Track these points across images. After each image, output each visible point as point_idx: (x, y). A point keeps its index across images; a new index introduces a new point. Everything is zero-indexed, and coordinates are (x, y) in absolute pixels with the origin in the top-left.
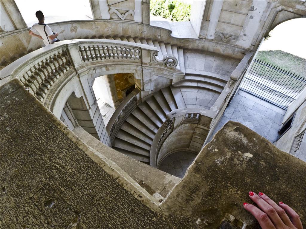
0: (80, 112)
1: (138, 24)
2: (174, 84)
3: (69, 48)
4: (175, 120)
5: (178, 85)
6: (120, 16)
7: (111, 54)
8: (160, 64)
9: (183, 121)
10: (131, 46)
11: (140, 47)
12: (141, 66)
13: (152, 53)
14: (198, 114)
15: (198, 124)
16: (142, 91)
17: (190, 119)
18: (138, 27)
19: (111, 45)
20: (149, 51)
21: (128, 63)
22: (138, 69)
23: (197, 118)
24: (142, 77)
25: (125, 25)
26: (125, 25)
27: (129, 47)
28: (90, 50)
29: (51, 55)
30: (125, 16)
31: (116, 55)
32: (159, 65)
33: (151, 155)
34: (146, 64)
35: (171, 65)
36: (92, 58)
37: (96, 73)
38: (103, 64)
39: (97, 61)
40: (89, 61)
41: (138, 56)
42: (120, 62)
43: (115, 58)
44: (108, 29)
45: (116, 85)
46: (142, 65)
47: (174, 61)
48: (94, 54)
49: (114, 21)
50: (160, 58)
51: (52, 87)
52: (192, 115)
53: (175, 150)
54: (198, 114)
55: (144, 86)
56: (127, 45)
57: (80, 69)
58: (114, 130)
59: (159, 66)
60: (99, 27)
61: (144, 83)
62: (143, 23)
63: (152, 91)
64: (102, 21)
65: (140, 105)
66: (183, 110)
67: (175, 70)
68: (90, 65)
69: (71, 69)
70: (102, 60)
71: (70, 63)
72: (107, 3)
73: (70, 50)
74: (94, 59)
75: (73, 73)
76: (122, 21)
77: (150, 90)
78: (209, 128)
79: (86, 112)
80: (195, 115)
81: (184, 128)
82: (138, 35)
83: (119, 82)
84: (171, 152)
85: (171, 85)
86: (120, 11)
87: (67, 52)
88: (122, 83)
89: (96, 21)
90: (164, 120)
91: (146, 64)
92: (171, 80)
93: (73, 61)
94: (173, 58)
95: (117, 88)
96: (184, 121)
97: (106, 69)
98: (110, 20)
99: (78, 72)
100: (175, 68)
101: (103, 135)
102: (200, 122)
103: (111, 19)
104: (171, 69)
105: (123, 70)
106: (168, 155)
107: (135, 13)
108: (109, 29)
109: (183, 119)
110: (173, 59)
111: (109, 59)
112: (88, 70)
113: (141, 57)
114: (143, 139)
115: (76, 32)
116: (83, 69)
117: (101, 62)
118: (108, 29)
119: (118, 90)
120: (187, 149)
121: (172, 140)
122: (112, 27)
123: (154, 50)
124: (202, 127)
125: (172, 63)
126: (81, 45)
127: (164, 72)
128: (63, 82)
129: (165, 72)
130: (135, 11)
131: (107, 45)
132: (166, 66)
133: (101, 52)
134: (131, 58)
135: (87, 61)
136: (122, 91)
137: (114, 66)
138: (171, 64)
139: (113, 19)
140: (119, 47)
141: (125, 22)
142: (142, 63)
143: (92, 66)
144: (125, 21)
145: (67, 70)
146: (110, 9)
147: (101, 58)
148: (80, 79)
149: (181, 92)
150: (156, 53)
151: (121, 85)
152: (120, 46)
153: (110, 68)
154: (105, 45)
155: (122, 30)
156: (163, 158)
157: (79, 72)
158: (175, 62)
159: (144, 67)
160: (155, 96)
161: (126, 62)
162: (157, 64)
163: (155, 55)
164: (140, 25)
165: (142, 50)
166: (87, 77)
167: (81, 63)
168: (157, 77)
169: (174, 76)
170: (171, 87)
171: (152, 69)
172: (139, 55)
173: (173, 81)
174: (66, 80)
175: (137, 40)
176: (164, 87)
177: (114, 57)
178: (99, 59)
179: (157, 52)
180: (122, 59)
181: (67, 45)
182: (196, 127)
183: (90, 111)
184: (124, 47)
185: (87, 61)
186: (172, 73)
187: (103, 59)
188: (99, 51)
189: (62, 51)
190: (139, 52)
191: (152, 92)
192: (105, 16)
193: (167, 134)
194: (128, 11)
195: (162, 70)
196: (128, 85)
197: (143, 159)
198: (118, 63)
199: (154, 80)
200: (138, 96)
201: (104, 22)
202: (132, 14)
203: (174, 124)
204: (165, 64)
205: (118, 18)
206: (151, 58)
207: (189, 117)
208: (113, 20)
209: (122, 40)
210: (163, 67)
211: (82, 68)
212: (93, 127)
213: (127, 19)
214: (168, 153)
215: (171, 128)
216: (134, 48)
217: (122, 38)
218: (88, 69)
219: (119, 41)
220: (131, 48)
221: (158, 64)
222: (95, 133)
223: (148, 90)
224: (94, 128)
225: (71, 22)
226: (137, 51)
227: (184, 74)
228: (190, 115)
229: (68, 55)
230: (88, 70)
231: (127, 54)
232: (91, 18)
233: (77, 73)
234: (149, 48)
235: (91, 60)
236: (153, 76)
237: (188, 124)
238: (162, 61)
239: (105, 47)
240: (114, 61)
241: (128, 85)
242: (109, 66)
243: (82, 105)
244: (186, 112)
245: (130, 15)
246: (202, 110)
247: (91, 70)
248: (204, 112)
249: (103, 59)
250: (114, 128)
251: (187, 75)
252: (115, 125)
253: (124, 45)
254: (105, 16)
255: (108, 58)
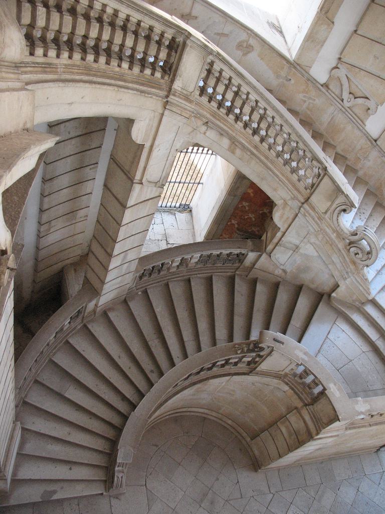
0: (121, 176)
1: (367, 135)
2: (334, 297)
3: (188, 42)
4: (270, 354)
5: (339, 307)
6: (346, 95)
7: (262, 129)
8: (339, 233)
9: (283, 373)
10: (311, 151)
11: (326, 167)
12: (300, 204)
13: (341, 199)
14: (304, 365)
15: (306, 405)
16: (267, 253)
17: (299, 381)
18: (363, 142)
19: (275, 114)
20: (338, 190)
21: (280, 176)
22: (290, 203)
23: (314, 394)
24: (286, 226)
25: (340, 118)
26: (340, 118)
27: (305, 148)
28: (218, 80)
29: (144, 22)
30: (354, 102)
31: (271, 140)
32: (335, 235)
33: (170, 374)
34: (313, 209)
35: (358, 254)
36: (220, 104)
37: (205, 133)
38: (230, 132)
39: (225, 117)
40: (209, 102)
41: (310, 181)
42: (267, 158)
43: (264, 144)
44: (304, 99)
45: (236, 208)
46: (303, 203)
47: (368, 253)
48: (222, 93)
49: (327, 93)
50: (348, 221)
51: (95, 65)
52: (309, 379)
53: (225, 419)
54: (304, 365)
55: (277, 248)
56: (305, 141)
57: (179, 97)
58: (156, 275)
59: (334, 236)
60: (293, 81)
61: (280, 242)
62: (378, 142)
63: (284, 271)
64: (306, 75)
65: (237, 274)
66: (301, 351)
67: (358, 270)
68: (207, 112)
69: (162, 81)
70: (236, 126)
71: (170, 70)
72: (341, 54)
73: (188, 49)
74: (223, 108)
75: (160, 89)
76: (342, 106)
77: (282, 267)
78: (318, 434)
79: (130, 182)
80: (316, 382)
81: (275, 387)
82: (351, 156)
83: (247, 208)
84: (214, 414)
85: (329, 296)
86: (353, 87)
87: (180, 48)
88: (250, 215)
89: (295, 68)
90: (254, 336)
91: (313, 209)
92: (336, 286)
93: (179, 72)
94: (373, 246)
95: (234, 215)
96: (286, 375)
97: (230, 147)
98: (322, 86)
99: (171, 97)
100: (362, 269)
101: (125, 258)
102: (313, 405)
103: (326, 85)
104: (354, 263)
105: (262, 179)
106: (204, 415)
107: (376, 112)
108: (306, 100)
109: (287, 371)
110: (370, 246)
111: (251, 136)
112: (193, 113)
113: (313, 187)
114: (185, 339)
115: (245, 54)
116: (184, 102)
117: (232, 125)
118: (300, 99)
119: (233, 222)
120: (248, 439)
121: (234, 391)
122: (315, 100)
123: (347, 196)
124: (307, 418)
125: (362, 253)
126: (217, 61)
127: (335, 255)
128: (125, 81)
129: (335, 258)
130: (379, 107)
131: (250, 91)
132: (348, 247)
133: (247, 109)
134: (294, 171)
135: (205, 99)
136: (238, 229)
137: (249, 153)
138: (360, 252)
139: (329, 89)
140: (287, 132)
141: (347, 113)
142: (307, 200)
143: (208, 116)
144: (346, 110)
145: (153, 74)
146: (336, 67)
147: (238, 118)
148: (164, 112)
149: (334, 323)
150: (347, 206)
151: (246, 217)
152: (290, 132)
153: (238, 152)
154: (262, 104)
155: (330, 121)
156: (189, 409)
157: (172, 98)
158: (370, 255)
159: (304, 209)
160: (281, 288)
161: (278, 170)
162: (333, 229)
163: (343, 207)
164: (368, 141)
165: (326, 177)
166: (181, 124)
167: (191, 89)
168: (316, 254)
169: (348, 281)
170: (325, 297)
171: (316, 227)
172: (314, 182)
173: (339, 289)
174: (135, 86)
175: (330, 150)
176: (312, 286)
177: (262, 140)
178: (232, 117)
179: (353, 206)
180: (276, 159)
181: (189, 36)
182: (296, 408)
183: (137, 188)
184: (297, 139)
185: (205, 99)
186: (347, 273)
187: (240, 124)
188: (244, 103)
189: (173, 37)
190: (319, 175)
191: (283, 274)
192: (320, 72)
193: (234, 369)
194: (367, 98)
195: (335, 248)
196: (258, 231)
197: (152, 371)
198: (263, 158)
199: (305, 254)
200: (252, 256)
201: (309, 80)
202: (369, 109)
203: (262, 361)
204: (350, 243)
205: (339, 96)
206: (331, 206)
207: (301, 377)
208: (327, 91)
209: (324, 150)
210: (341, 245)
211: (184, 100)
212: (118, 223)
213: (354, 110)
214: (206, 411)
215: (252, 365)
216: (315, 158)
217: (316, 135)
218: (195, 112)
219: (307, 136)
220: (309, 155)
221: (334, 231)
222: (113, 238)
223: (278, 265)
224: (118, 227)
225: (249, 32)
226: (316, 170)
227: (370, 298)
228: (307, 372)
229: (178, 53)
230: (193, 113)
231: (300, 165)
232: (289, 50)
233: (167, 97)
234: (343, 185)
235: (214, 104)
236: (309, 245)
237: (286, 388)
238: (348, 233)
239: (260, 108)
240: (256, 147)
241: (258, 231)
242: (240, 146)
243: (132, 163)
244: (303, 360)
245: (367, 108)
246: (335, 385)
247: (199, 118)
248: (335, 392)
249: (240, 124)
250: (159, 271)
251: (374, 303)
252: (165, 267)
253: (300, 136)
254: (320, 72)
255: (251, 132)
